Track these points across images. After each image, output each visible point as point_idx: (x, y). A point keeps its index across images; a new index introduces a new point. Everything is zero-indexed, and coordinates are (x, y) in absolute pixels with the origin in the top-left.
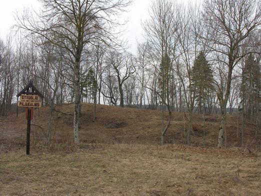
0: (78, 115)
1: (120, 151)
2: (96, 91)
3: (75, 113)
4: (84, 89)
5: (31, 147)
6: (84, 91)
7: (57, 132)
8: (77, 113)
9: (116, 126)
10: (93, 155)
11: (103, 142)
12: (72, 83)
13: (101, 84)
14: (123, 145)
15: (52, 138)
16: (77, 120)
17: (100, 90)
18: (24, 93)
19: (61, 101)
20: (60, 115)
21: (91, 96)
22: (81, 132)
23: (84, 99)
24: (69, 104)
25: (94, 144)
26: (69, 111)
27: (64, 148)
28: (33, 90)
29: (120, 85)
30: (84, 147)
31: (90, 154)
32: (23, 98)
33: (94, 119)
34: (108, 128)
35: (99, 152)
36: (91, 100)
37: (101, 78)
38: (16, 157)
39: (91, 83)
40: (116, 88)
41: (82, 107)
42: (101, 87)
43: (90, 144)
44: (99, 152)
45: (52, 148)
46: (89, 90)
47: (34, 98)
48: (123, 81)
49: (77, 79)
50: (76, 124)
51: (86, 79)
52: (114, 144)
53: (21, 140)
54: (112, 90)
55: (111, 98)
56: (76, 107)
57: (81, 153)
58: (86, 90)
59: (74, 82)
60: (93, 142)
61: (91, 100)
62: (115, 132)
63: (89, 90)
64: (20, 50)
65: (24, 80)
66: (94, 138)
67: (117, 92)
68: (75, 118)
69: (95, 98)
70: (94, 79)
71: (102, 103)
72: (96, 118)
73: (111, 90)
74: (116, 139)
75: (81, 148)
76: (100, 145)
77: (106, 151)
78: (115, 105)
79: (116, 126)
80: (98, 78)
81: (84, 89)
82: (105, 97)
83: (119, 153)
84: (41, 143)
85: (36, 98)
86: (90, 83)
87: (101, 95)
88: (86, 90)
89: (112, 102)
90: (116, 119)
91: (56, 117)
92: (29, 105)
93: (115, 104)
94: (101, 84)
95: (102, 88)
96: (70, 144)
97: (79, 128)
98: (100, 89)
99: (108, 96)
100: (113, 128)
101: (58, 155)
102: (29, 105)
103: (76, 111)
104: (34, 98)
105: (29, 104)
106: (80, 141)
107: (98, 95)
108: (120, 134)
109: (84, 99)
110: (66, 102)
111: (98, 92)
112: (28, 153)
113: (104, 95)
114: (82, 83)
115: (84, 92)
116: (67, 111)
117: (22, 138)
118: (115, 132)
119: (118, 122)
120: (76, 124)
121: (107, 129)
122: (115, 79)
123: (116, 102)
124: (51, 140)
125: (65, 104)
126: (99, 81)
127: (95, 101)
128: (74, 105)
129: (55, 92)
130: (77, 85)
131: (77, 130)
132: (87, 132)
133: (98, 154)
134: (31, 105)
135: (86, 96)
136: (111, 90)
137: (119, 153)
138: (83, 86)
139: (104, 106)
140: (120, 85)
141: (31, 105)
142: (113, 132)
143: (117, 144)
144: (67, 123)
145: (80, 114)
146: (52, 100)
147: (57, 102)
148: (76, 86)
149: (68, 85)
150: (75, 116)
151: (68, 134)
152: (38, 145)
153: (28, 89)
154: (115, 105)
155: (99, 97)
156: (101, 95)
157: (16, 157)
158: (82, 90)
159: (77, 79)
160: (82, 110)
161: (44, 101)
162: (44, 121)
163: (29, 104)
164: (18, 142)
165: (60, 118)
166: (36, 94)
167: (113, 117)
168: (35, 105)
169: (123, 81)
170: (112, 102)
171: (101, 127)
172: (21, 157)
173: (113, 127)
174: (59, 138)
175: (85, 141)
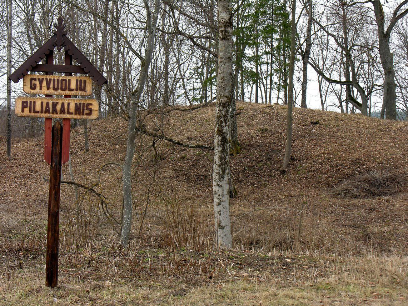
0: (229, 145)
1: (385, 279)
2: (293, 59)
3: (217, 140)
4: (249, 52)
5: (62, 260)
6: (250, 59)
7: (151, 211)
8: (224, 141)
9: (365, 190)
10: (288, 291)
11: (319, 245)
12: (203, 31)
13: (309, 36)
14: (394, 258)
15: (135, 232)
16: (223, 164)
17: (306, 55)
18: (36, 68)
19: (166, 98)
20: (161, 146)
21: (275, 79)
22: (236, 208)
23: (249, 89)
24: (193, 108)
25: (288, 253)
26: (195, 134)
27: (179, 265)
28: (69, 57)
29: (384, 37)
30: (249, 264)
31: (273, 290)
32: (33, 87)
33: (285, 161)
34: (336, 195)
35: (309, 283)
36: (275, 92)
37: (310, 13)
38: (8, 296)
39: (273, 31)
40: (366, 48)
41: (242, 121)
42: (309, 45)
43: (275, 253)
44: (309, 283)
45: (135, 264)
46: (265, 58)
47: (73, 85)
48: (396, 18)
49: (225, 16)
50: (221, 177)
51: (255, 18)
52: (358, 253)
53: (26, 236)
54: (354, 54)
55: (350, 84)
56: (223, 118)
57: (241, 284)
58: (256, 59)
59: (213, 28)
60: (281, 245)
61: (275, 92)
62: (362, 212)
63: (265, 58)
64: (160, 52)
65: (29, 22)
66: (288, 233)
67: (371, 62)
68: (216, 159)
69: (288, 87)
70: (286, 16)
71: (313, 103)
72: (292, 159)
73: (348, 56)
74: (366, 237)
75: (239, 266)
76: (311, 259)
77: (332, 279)
78: (364, 113)
79: (365, 190)
80: (298, 11)
81: (249, 52)
82: (325, 83)
83: (380, 290)
84: (97, 245)
85: (81, 87)
86: (269, 31)
87: (312, 73)
88: (256, 59)
89: (351, 98)
90: (368, 165)
91: (147, 155)
92: (55, 111)
93: (363, 107)
94: (309, 36)
95: (315, 50)
96: (199, 252)
97: (233, 194)
98: (308, 52)
99: (335, 76)
100: (355, 197)
101: (157, 289)
102: (55, 111)
103: (220, 132)
104: (73, 85)
105: (55, 105)
106: (237, 241)
107: (297, 74)
108: (383, 219)
109: (249, 89)
110: (182, 101)
111: (299, 65)
112: (51, 280)
113: (320, 73)
114: (239, 30)
115: (248, 65)
116: (188, 134)
117: (28, 230)
118: (362, 212)
119: (375, 174)
120: (221, 177)
121: (333, 200)
122: (363, 14)
123: (366, 98)
124: (129, 237)
125: (179, 108)
126: (302, 23)
127: (289, 100)
128: (212, 113)
129: (145, 64)
130: (225, 38)
131: (226, 204)
132: (260, 210)
133: (302, 289)
134: (62, 111)
135: (255, 77)
136: (348, 56)
137: (380, 290)
138: (242, 43)
139: (322, 113)
140: (384, 37)
141: (62, 111)
142: (355, 212)
143: (372, 256)
144: (186, 177)
145: (235, 144)
146: (136, 94)
147: (152, 104)
148: (221, 42)
149: (191, 38)
150: (218, 149)
151: (191, 216)
152: (85, 253)
153: (49, 56)
154: (364, 113)
155: (304, 83)
156: (312, 73)
157: (8, 296)
158: (241, 55)
159: (225, 16)
160: (240, 131)
161: (104, 98)
162: (106, 168)
163: (55, 105)
164: (14, 243)
165: (161, 157)
166: (81, 70)
167: (355, 155)
168: (78, 110)
169: (396, 18)
170: (351, 98)
171: (313, 192)
172: (29, 294)
173: (355, 191)
174: (158, 231)
175: (250, 243)
